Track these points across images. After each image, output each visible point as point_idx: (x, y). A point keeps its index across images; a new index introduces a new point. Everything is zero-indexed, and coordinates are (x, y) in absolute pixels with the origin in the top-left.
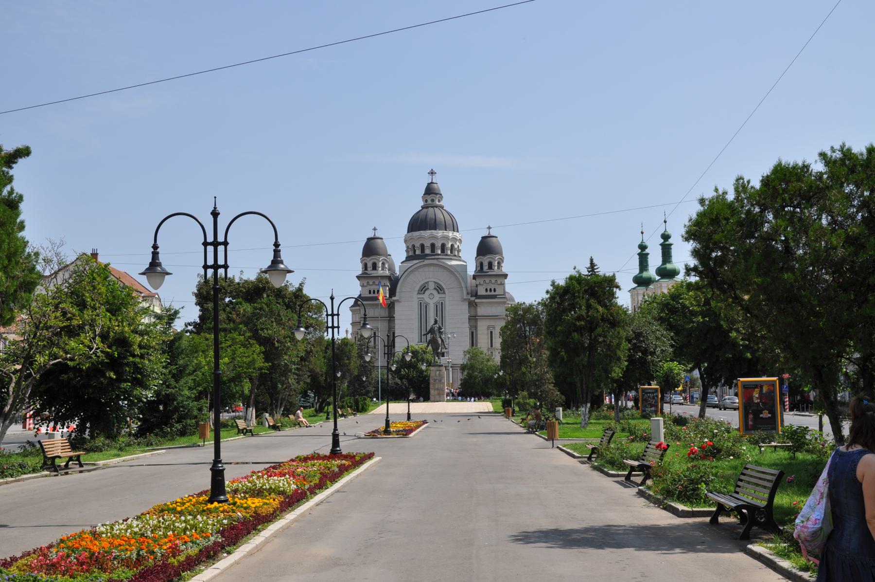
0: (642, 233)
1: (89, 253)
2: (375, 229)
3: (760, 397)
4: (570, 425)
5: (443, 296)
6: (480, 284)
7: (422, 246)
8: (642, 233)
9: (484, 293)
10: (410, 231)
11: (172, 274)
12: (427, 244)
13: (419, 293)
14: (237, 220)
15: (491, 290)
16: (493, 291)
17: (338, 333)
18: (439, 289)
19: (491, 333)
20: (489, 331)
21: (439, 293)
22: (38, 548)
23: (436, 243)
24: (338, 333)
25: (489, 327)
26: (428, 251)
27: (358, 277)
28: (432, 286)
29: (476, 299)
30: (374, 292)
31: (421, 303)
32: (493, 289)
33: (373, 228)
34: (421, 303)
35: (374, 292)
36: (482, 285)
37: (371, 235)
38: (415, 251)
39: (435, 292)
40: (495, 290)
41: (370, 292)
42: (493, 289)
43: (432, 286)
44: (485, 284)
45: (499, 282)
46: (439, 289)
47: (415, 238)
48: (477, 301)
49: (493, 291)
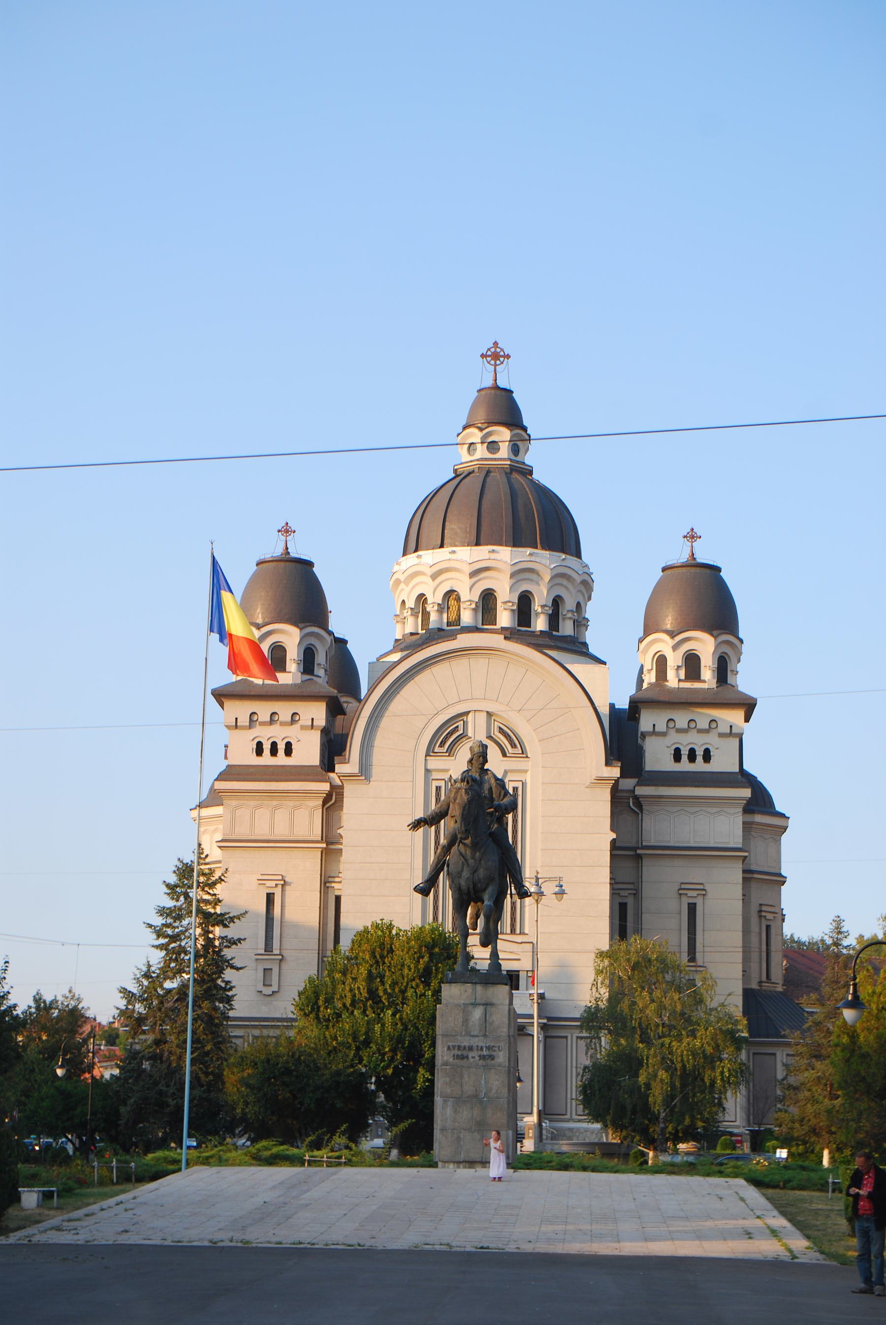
3: (248, 1046)
6: (654, 733)
9: (668, 765)
11: (604, 663)
13: (430, 752)
14: (456, 492)
16: (700, 759)
17: (772, 906)
19: (692, 908)
20: (685, 901)
21: (504, 754)
22: (157, 1228)
23: (697, 749)
24: (772, 906)
25: (681, 892)
29: (639, 784)
30: (692, 756)
32: (700, 753)
35: (692, 756)
36: (663, 734)
38: (426, 615)
42: (700, 753)
44: (672, 732)
45: (703, 724)
47: (402, 578)
48: (641, 791)
49: (700, 759)
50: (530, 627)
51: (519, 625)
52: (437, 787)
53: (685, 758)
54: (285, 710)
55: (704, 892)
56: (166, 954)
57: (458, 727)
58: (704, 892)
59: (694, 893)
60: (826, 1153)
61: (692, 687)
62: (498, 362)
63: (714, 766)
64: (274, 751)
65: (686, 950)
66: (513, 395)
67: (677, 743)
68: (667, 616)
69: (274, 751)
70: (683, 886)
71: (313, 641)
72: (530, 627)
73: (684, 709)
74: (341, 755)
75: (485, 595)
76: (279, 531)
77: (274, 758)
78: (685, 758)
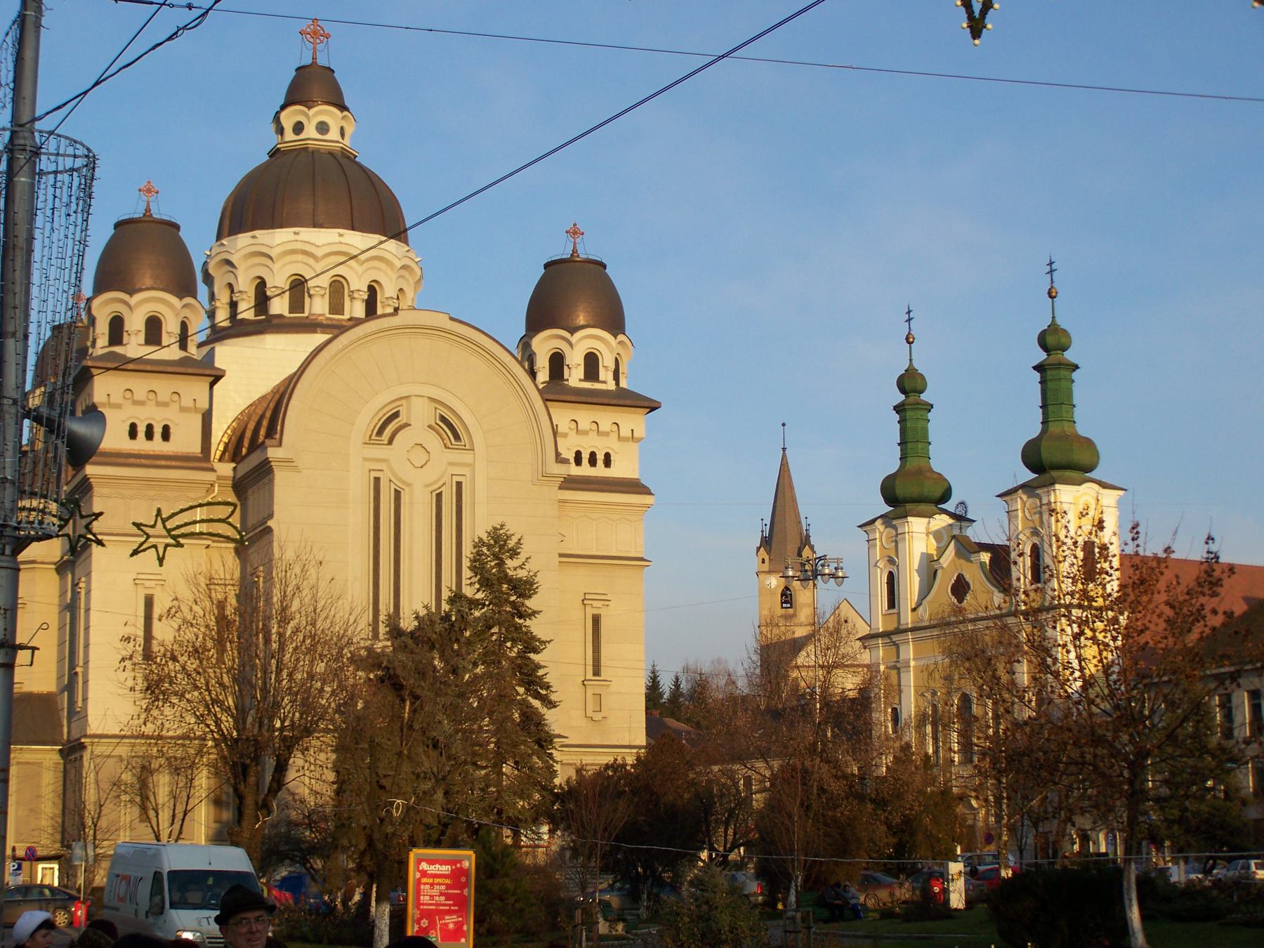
0: (909, 340)
1: (553, 697)
2: (575, 232)
4: (160, 822)
5: (466, 457)
7: (337, 289)
8: (909, 340)
10: (226, 230)
11: (132, 555)
12: (278, 279)
15: (593, 460)
18: (450, 428)
19: (596, 620)
26: (279, 306)
27: (899, 444)
28: (420, 415)
30: (593, 460)
31: (377, 480)
33: (569, 226)
34: (377, 480)
37: (561, 250)
39: (433, 442)
40: (608, 461)
41: (133, 433)
43: (420, 415)
44: (593, 435)
46: (450, 428)
50: (343, 315)
51: (290, 313)
52: (375, 478)
53: (600, 462)
54: (164, 386)
55: (163, 583)
56: (1121, 731)
57: (398, 412)
58: (163, 583)
59: (152, 584)
60: (375, 886)
61: (593, 387)
62: (318, 41)
63: (616, 472)
64: (149, 434)
65: (591, 663)
66: (335, 75)
67: (613, 449)
68: (578, 316)
69: (149, 434)
70: (140, 577)
71: (187, 313)
72: (343, 315)
73: (586, 410)
74: (273, 438)
75: (334, 281)
76: (140, 190)
77: (149, 443)
78: (600, 462)
